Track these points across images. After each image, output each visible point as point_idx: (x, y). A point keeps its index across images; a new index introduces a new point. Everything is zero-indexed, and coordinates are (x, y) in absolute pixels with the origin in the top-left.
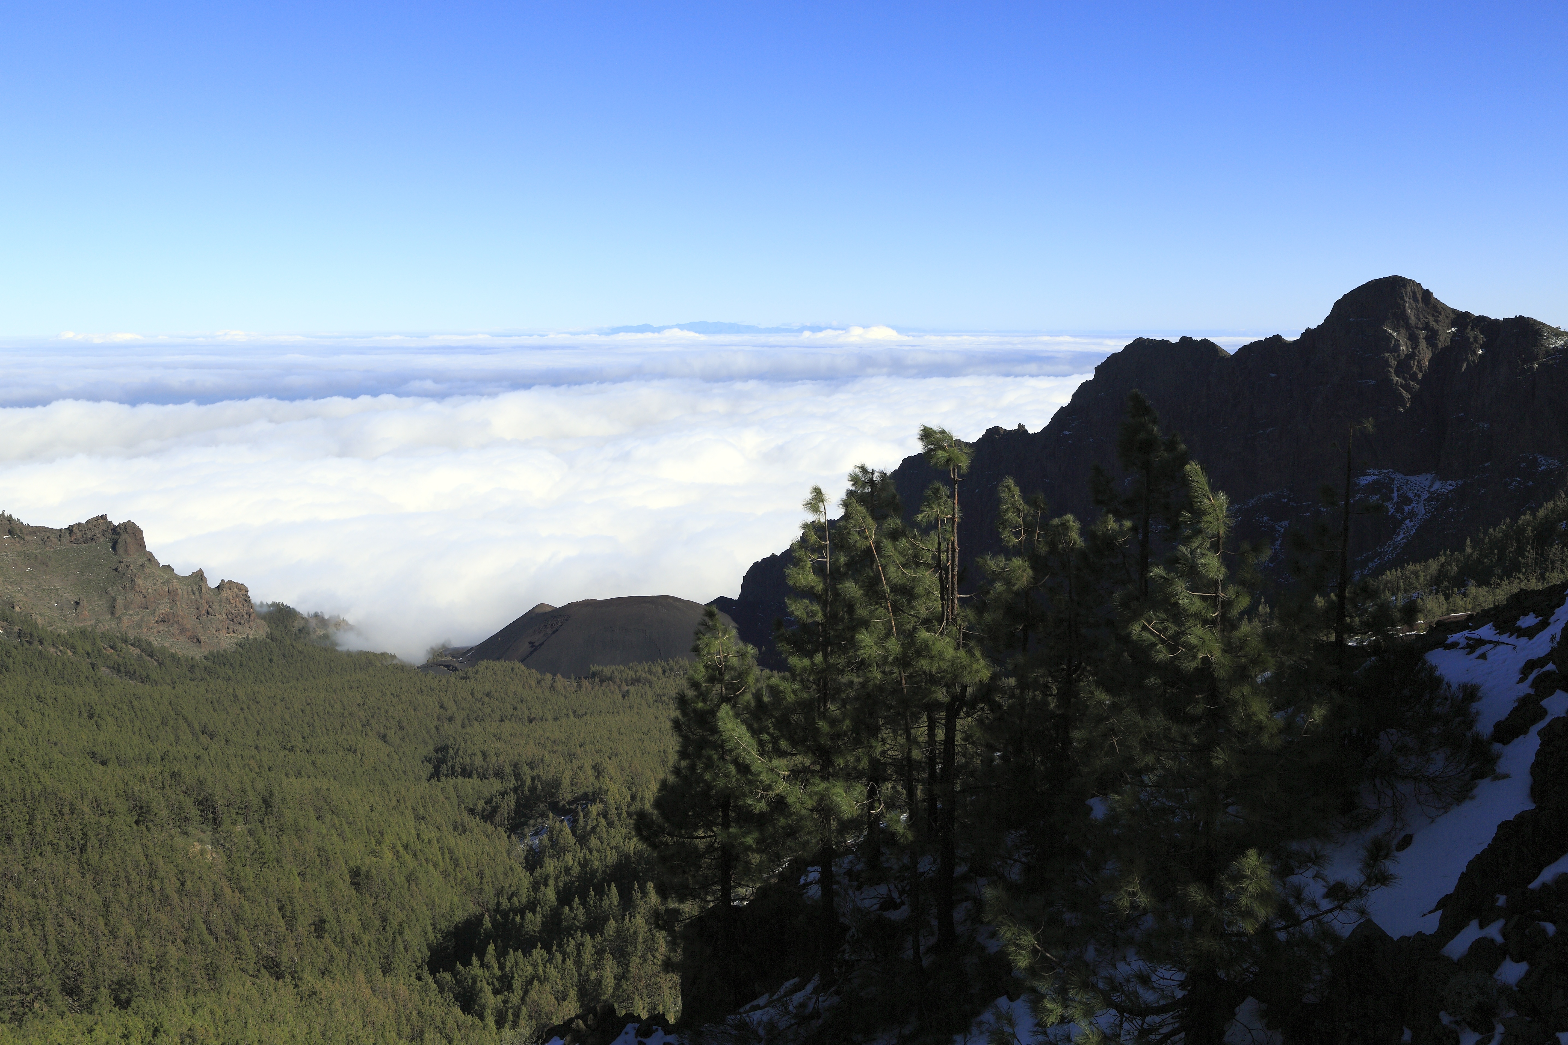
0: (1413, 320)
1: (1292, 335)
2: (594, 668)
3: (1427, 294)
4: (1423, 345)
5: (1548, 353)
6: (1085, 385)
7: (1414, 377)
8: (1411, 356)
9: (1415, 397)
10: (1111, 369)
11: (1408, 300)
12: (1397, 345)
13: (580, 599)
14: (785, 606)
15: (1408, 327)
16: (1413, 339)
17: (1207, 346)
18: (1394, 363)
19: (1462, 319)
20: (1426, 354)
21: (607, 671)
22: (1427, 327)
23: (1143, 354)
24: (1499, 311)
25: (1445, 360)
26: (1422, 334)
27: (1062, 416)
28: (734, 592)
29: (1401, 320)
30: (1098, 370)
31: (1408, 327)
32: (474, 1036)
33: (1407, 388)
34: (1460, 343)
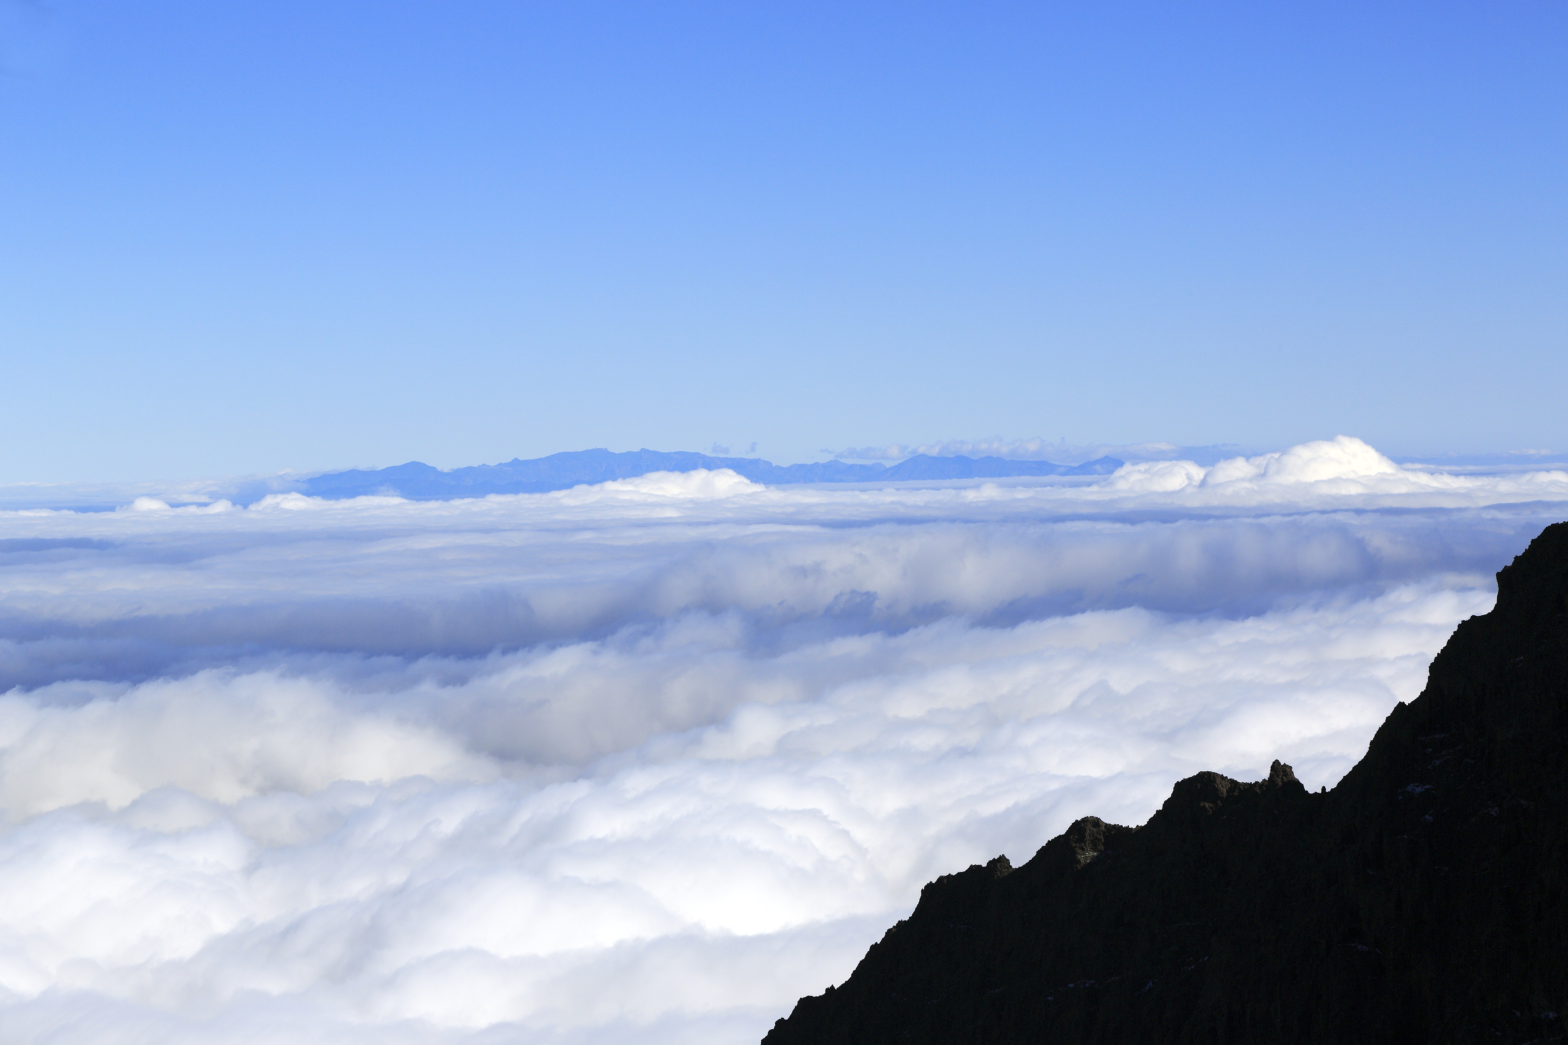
6: (1469, 632)
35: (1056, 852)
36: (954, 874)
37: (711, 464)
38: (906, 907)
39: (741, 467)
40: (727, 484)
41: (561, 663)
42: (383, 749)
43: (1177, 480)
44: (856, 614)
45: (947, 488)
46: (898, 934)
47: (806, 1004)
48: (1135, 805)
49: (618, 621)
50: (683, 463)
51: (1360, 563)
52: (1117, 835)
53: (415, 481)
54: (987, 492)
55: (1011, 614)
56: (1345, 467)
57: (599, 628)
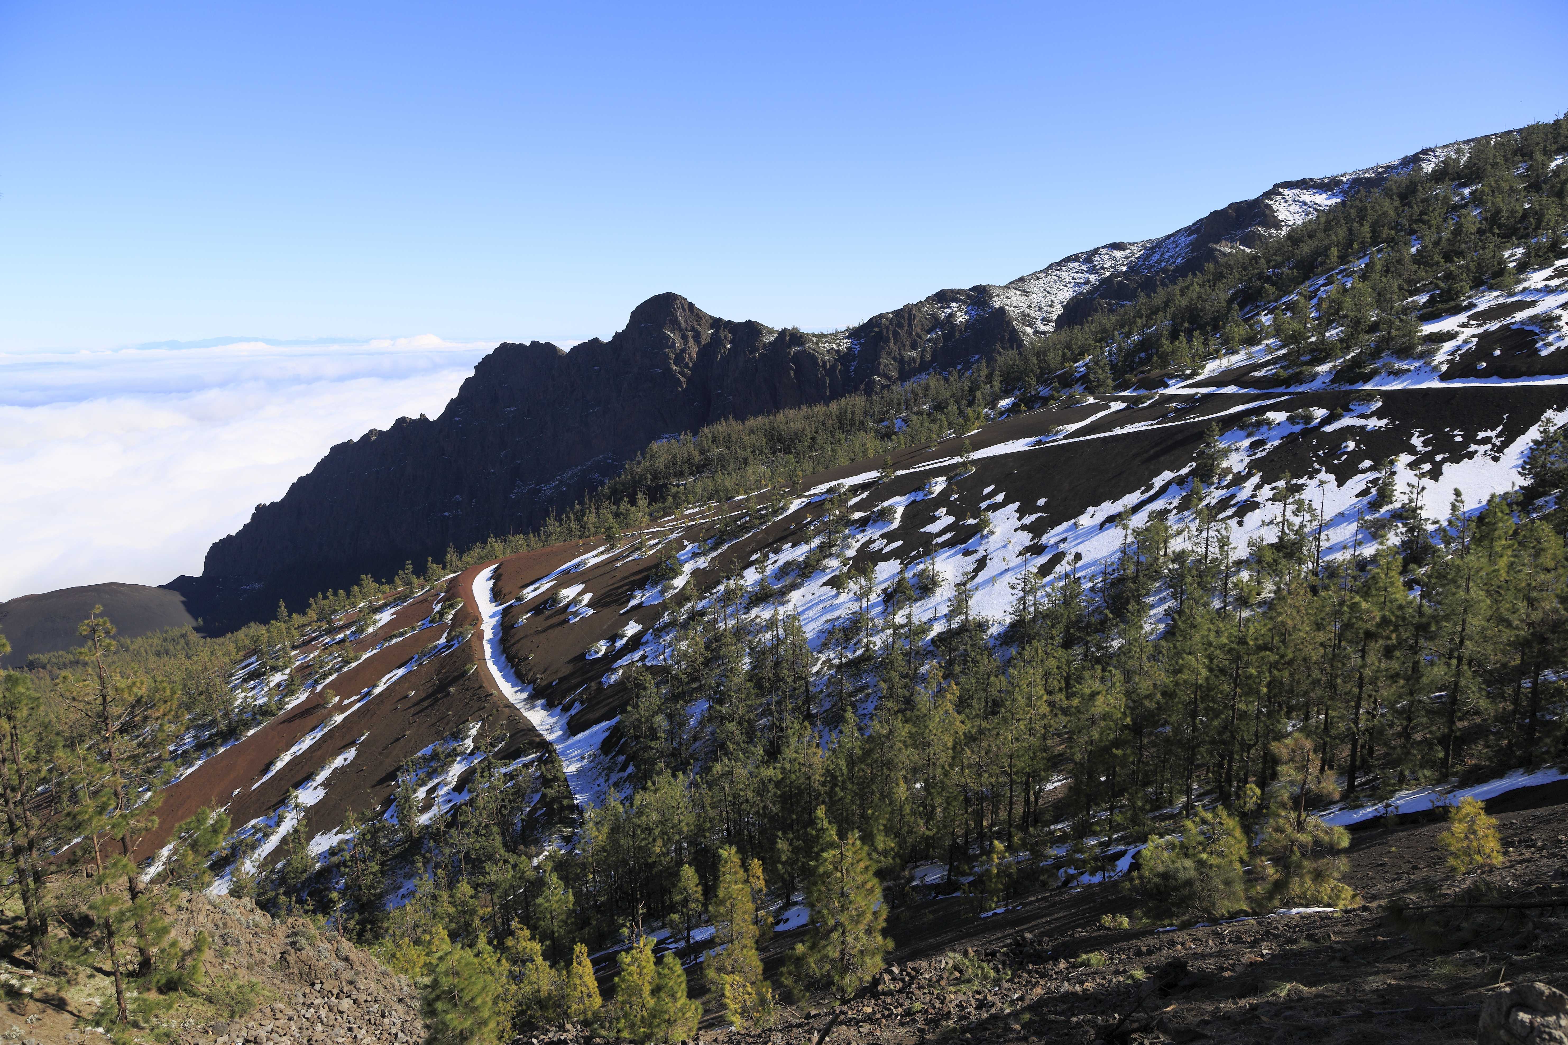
0: (683, 324)
1: (606, 337)
2: (31, 657)
3: (691, 305)
4: (691, 342)
5: (765, 345)
6: (468, 381)
7: (687, 366)
8: (683, 351)
9: (689, 380)
10: (486, 366)
11: (679, 310)
12: (674, 343)
13: (19, 595)
14: (445, 553)
15: (680, 329)
16: (684, 338)
17: (549, 348)
18: (672, 356)
19: (717, 323)
20: (694, 349)
21: (43, 658)
22: (693, 329)
23: (507, 354)
24: (738, 317)
25: (707, 352)
26: (690, 334)
27: (453, 405)
28: (197, 570)
29: (675, 324)
30: (476, 368)
31: (680, 329)
32: (1567, 330)
33: (682, 374)
34: (716, 340)
35: (366, 438)
36: (278, 494)
37: (256, 340)
38: (326, 453)
39: (268, 341)
40: (261, 345)
41: (212, 394)
42: (163, 418)
43: (384, 345)
44: (297, 380)
45: (12, 404)
46: (324, 460)
47: (300, 478)
48: (386, 425)
49: (228, 382)
50: (248, 340)
51: (435, 365)
52: (381, 433)
53: (173, 345)
54: (335, 347)
55: (341, 379)
56: (429, 342)
57: (223, 384)
